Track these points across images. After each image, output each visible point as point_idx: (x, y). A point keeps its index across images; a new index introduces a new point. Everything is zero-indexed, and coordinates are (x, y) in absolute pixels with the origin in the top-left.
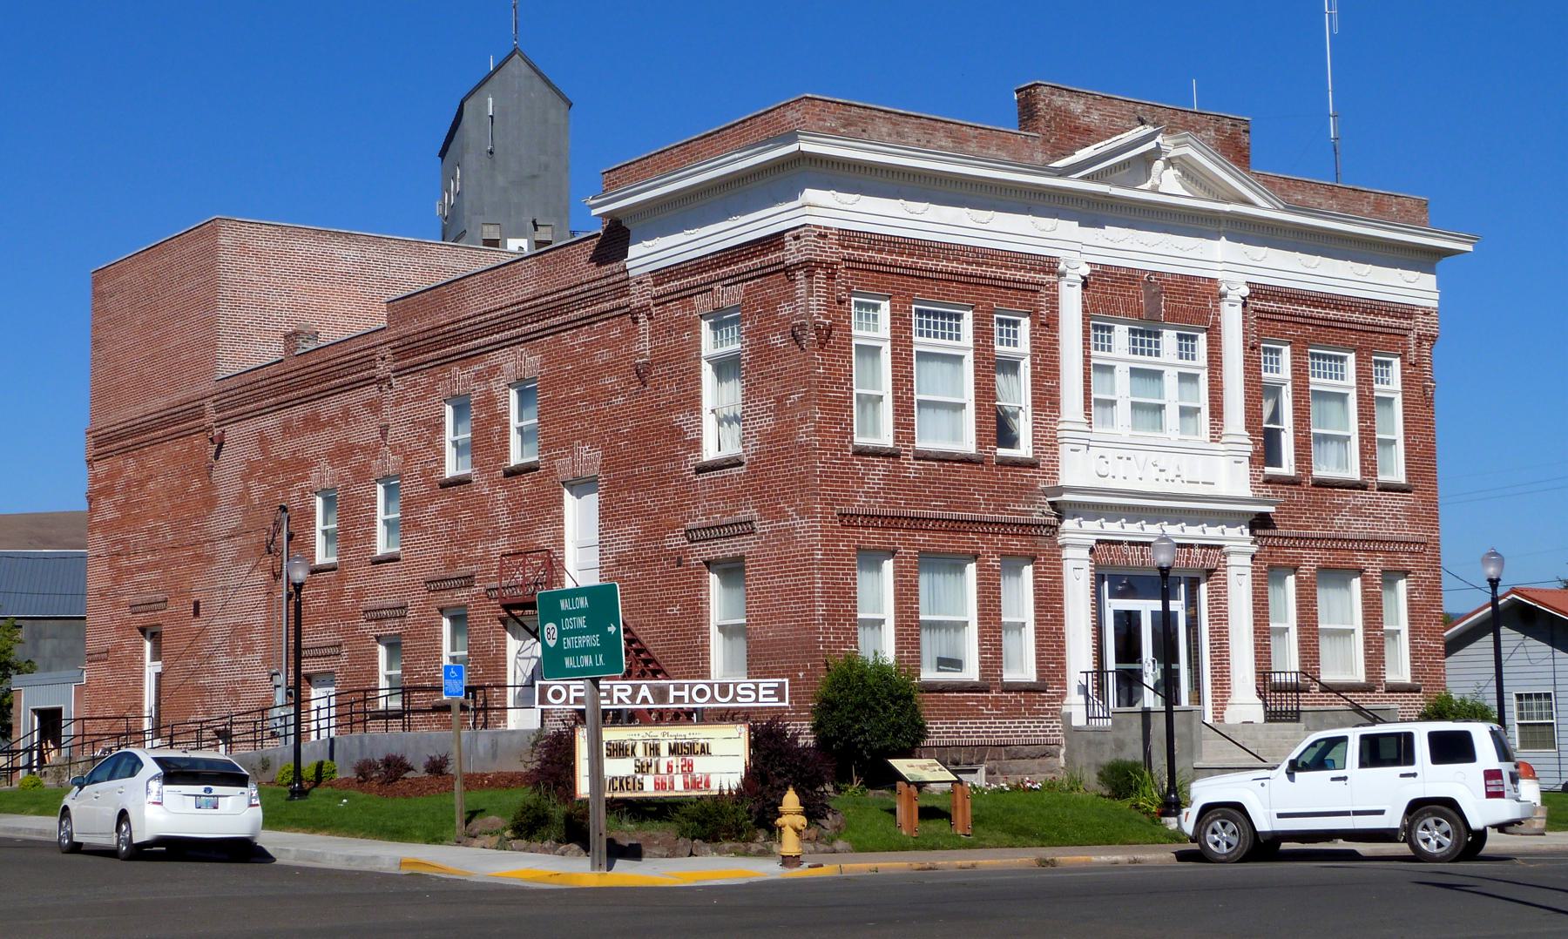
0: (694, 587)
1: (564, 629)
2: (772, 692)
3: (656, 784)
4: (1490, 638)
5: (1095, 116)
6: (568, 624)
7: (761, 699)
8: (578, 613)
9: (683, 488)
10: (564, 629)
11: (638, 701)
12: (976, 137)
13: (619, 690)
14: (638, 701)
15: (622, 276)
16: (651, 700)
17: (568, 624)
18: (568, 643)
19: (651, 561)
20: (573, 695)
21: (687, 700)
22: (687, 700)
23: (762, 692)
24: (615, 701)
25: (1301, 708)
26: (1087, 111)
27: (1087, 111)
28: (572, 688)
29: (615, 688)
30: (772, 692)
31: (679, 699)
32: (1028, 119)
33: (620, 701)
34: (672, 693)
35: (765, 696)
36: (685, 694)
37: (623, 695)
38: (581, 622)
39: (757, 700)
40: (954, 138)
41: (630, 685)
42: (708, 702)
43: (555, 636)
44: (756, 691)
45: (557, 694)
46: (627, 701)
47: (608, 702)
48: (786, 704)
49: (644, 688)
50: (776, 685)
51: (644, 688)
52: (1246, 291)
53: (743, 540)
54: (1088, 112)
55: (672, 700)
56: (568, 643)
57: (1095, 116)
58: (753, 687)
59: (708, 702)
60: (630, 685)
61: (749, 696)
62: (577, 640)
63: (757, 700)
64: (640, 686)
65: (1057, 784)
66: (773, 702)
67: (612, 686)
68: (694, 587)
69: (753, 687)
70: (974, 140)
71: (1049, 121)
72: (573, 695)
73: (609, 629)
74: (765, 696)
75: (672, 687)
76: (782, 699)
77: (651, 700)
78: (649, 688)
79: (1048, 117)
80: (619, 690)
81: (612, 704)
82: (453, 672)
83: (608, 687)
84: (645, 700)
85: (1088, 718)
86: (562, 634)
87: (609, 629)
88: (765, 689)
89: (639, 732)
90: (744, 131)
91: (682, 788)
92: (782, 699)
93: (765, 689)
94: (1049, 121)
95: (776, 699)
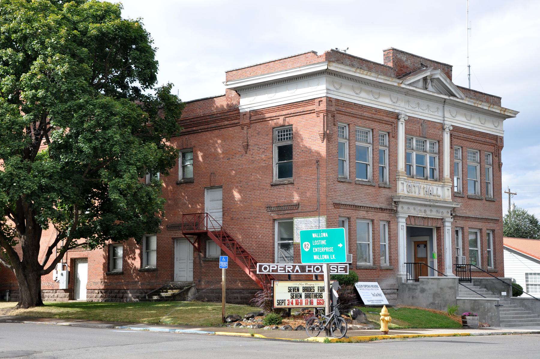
0: (268, 228)
1: (314, 244)
2: (343, 269)
3: (317, 302)
4: (506, 253)
5: (409, 62)
6: (316, 243)
7: (339, 271)
8: (323, 239)
9: (264, 192)
10: (314, 244)
11: (295, 272)
12: (374, 68)
13: (288, 267)
14: (295, 272)
15: (236, 112)
16: (299, 271)
17: (316, 243)
18: (316, 250)
19: (248, 219)
20: (271, 269)
21: (312, 271)
22: (312, 271)
23: (339, 269)
24: (287, 271)
25: (472, 278)
26: (407, 60)
27: (407, 60)
28: (271, 266)
29: (287, 266)
30: (343, 269)
31: (309, 271)
32: (388, 62)
33: (289, 272)
34: (307, 269)
35: (340, 270)
36: (312, 269)
37: (289, 269)
38: (324, 242)
39: (337, 272)
40: (368, 67)
41: (292, 265)
42: (320, 272)
43: (309, 247)
44: (337, 269)
45: (265, 268)
46: (291, 272)
47: (284, 272)
48: (348, 274)
49: (297, 266)
50: (344, 267)
51: (297, 266)
52: (451, 128)
53: (344, 214)
54: (407, 61)
55: (307, 271)
56: (316, 250)
57: (409, 62)
58: (336, 267)
59: (320, 272)
60: (292, 265)
61: (335, 270)
62: (321, 249)
63: (337, 272)
64: (296, 266)
65: (105, 300)
66: (343, 273)
67: (285, 265)
68: (268, 228)
69: (336, 267)
70: (374, 69)
71: (396, 63)
72: (271, 269)
73: (339, 245)
74: (340, 270)
75: (307, 266)
76: (346, 272)
77: (299, 271)
78: (299, 267)
79: (395, 62)
80: (288, 267)
81: (285, 272)
82: (223, 259)
83: (284, 266)
84: (297, 271)
85: (407, 280)
86: (312, 246)
87: (339, 245)
88: (340, 268)
89: (297, 283)
90: (295, 60)
91: (316, 304)
92: (346, 272)
93: (340, 268)
94: (396, 63)
95: (344, 272)
